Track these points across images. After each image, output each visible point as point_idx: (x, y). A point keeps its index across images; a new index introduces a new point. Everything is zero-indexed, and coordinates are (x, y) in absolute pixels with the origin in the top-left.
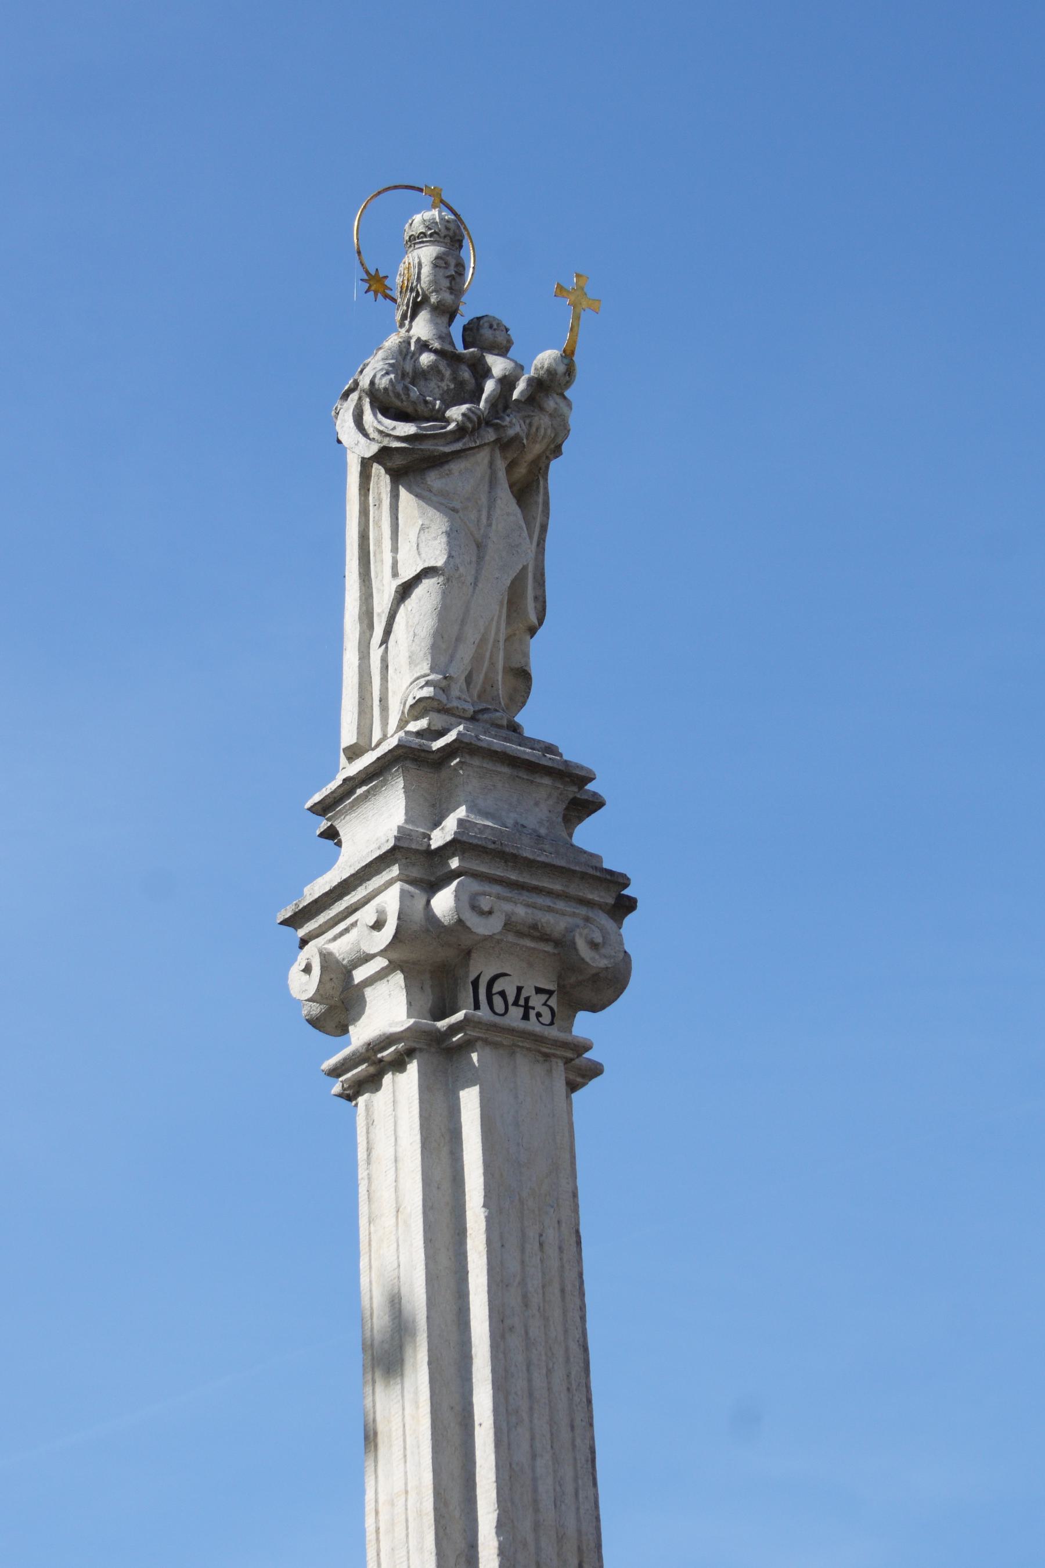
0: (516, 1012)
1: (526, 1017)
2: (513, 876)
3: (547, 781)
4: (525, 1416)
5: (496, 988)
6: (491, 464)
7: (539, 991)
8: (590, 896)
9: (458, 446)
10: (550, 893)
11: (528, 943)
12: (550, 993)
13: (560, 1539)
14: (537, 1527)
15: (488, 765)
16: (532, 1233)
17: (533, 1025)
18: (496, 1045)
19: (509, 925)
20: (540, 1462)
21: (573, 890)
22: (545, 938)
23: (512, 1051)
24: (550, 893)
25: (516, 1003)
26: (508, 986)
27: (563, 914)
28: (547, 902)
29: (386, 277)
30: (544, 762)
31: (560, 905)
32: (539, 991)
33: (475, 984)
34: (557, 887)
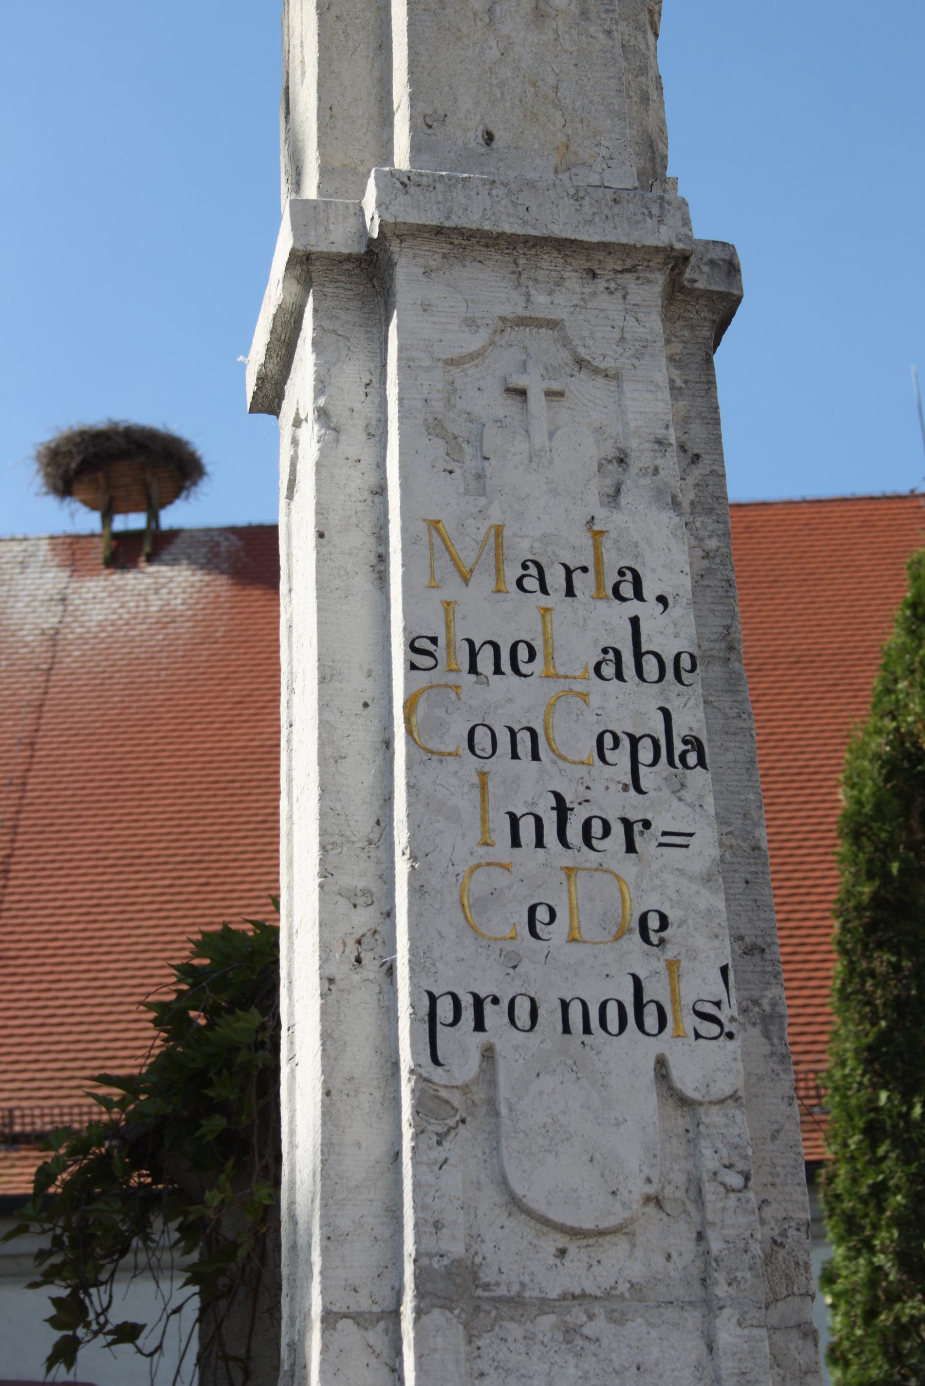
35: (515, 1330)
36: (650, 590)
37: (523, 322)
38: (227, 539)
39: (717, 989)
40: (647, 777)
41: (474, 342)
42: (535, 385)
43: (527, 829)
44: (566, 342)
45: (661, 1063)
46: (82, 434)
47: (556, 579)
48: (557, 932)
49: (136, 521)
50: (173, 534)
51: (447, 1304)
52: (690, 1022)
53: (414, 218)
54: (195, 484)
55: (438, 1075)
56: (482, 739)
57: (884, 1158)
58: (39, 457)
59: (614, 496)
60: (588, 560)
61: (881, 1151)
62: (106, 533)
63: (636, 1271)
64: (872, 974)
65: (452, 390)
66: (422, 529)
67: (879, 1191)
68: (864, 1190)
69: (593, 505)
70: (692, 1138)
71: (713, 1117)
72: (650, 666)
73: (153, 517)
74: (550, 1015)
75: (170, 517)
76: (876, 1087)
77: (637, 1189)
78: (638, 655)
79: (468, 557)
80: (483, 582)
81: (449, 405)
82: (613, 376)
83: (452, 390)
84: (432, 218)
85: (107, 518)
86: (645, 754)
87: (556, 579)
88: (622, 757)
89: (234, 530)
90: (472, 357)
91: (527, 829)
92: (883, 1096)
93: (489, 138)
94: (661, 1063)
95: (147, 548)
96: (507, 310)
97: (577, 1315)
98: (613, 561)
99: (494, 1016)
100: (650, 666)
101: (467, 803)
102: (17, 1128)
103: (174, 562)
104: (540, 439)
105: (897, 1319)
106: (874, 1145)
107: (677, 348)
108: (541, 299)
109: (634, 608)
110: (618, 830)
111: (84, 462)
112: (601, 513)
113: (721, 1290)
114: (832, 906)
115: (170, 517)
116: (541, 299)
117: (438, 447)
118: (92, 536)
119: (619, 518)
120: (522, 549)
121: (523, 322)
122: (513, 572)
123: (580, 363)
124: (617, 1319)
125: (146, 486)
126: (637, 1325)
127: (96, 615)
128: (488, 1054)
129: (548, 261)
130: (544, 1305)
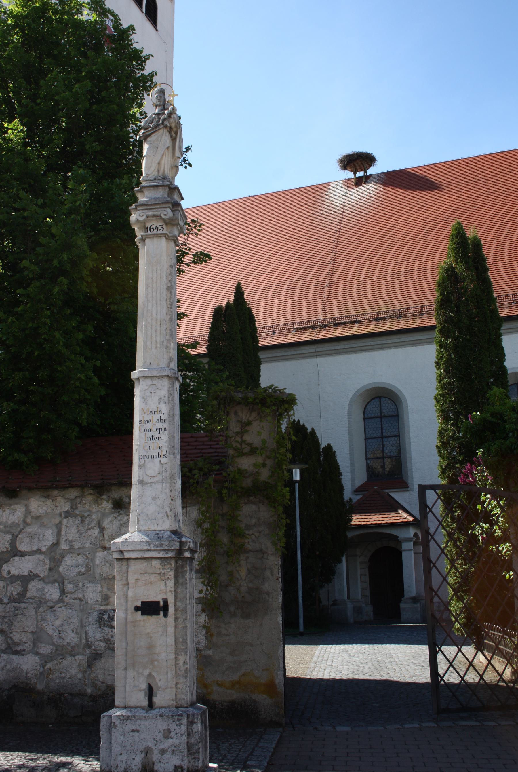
0: (155, 231)
1: (157, 231)
2: (149, 208)
3: (161, 187)
4: (151, 301)
5: (151, 227)
6: (163, 132)
7: (160, 225)
8: (165, 206)
9: (153, 131)
10: (158, 208)
11: (155, 218)
12: (163, 225)
13: (156, 320)
14: (152, 319)
15: (148, 189)
16: (155, 270)
17: (159, 232)
18: (150, 238)
19: (147, 217)
20: (153, 308)
21: (162, 206)
22: (157, 216)
23: (153, 237)
24: (158, 208)
25: (156, 229)
26: (154, 227)
27: (160, 211)
28: (157, 210)
29: (177, 95)
30: (158, 185)
31: (159, 210)
32: (160, 225)
33: (147, 228)
34: (158, 207)
35: (146, 486)
36: (162, 413)
37: (152, 385)
38: (382, 176)
39: (166, 453)
40: (161, 433)
41: (147, 388)
42: (152, 392)
43: (149, 439)
44: (156, 386)
45: (160, 461)
46: (347, 155)
47: (153, 413)
48: (151, 449)
49: (361, 174)
50: (370, 176)
51: (140, 484)
52: (163, 456)
53: (141, 376)
54: (375, 163)
55: (140, 463)
56: (146, 430)
57: (443, 351)
58: (338, 162)
59: (159, 404)
60: (156, 410)
61: (442, 350)
62: (355, 177)
63: (157, 480)
64: (441, 315)
65: (145, 393)
66: (141, 409)
67: (442, 357)
68: (439, 358)
69: (157, 404)
70: (163, 467)
71: (164, 465)
72: (162, 421)
73: (365, 172)
74: (150, 457)
75: (370, 172)
76: (442, 337)
77: (157, 472)
78: (161, 420)
79: (145, 411)
80: (147, 414)
81: (144, 395)
82: (160, 389)
83: (145, 393)
84: (142, 376)
85: (355, 174)
86: (161, 430)
87: (153, 413)
88: (158, 431)
89: (384, 173)
90: (147, 389)
91: (149, 439)
92: (443, 339)
93: (150, 363)
94: (160, 461)
95: (364, 181)
96: (150, 384)
97: (152, 484)
98: (159, 410)
99: (145, 457)
100: (162, 421)
101: (144, 437)
102: (337, 322)
103: (371, 183)
104: (153, 398)
105: (444, 382)
106: (441, 349)
107: (170, 383)
108: (154, 382)
109: (161, 415)
110: (158, 438)
111: (347, 162)
112: (158, 405)
113: (164, 481)
114: (434, 301)
115: (370, 172)
116: (154, 382)
117: (143, 400)
118: (352, 178)
119: (160, 405)
120: (150, 410)
121: (152, 385)
122: (149, 412)
123: (158, 388)
124: (155, 484)
125: (363, 165)
126: (157, 485)
127: (353, 198)
128: (145, 461)
129: (154, 378)
130: (149, 483)
